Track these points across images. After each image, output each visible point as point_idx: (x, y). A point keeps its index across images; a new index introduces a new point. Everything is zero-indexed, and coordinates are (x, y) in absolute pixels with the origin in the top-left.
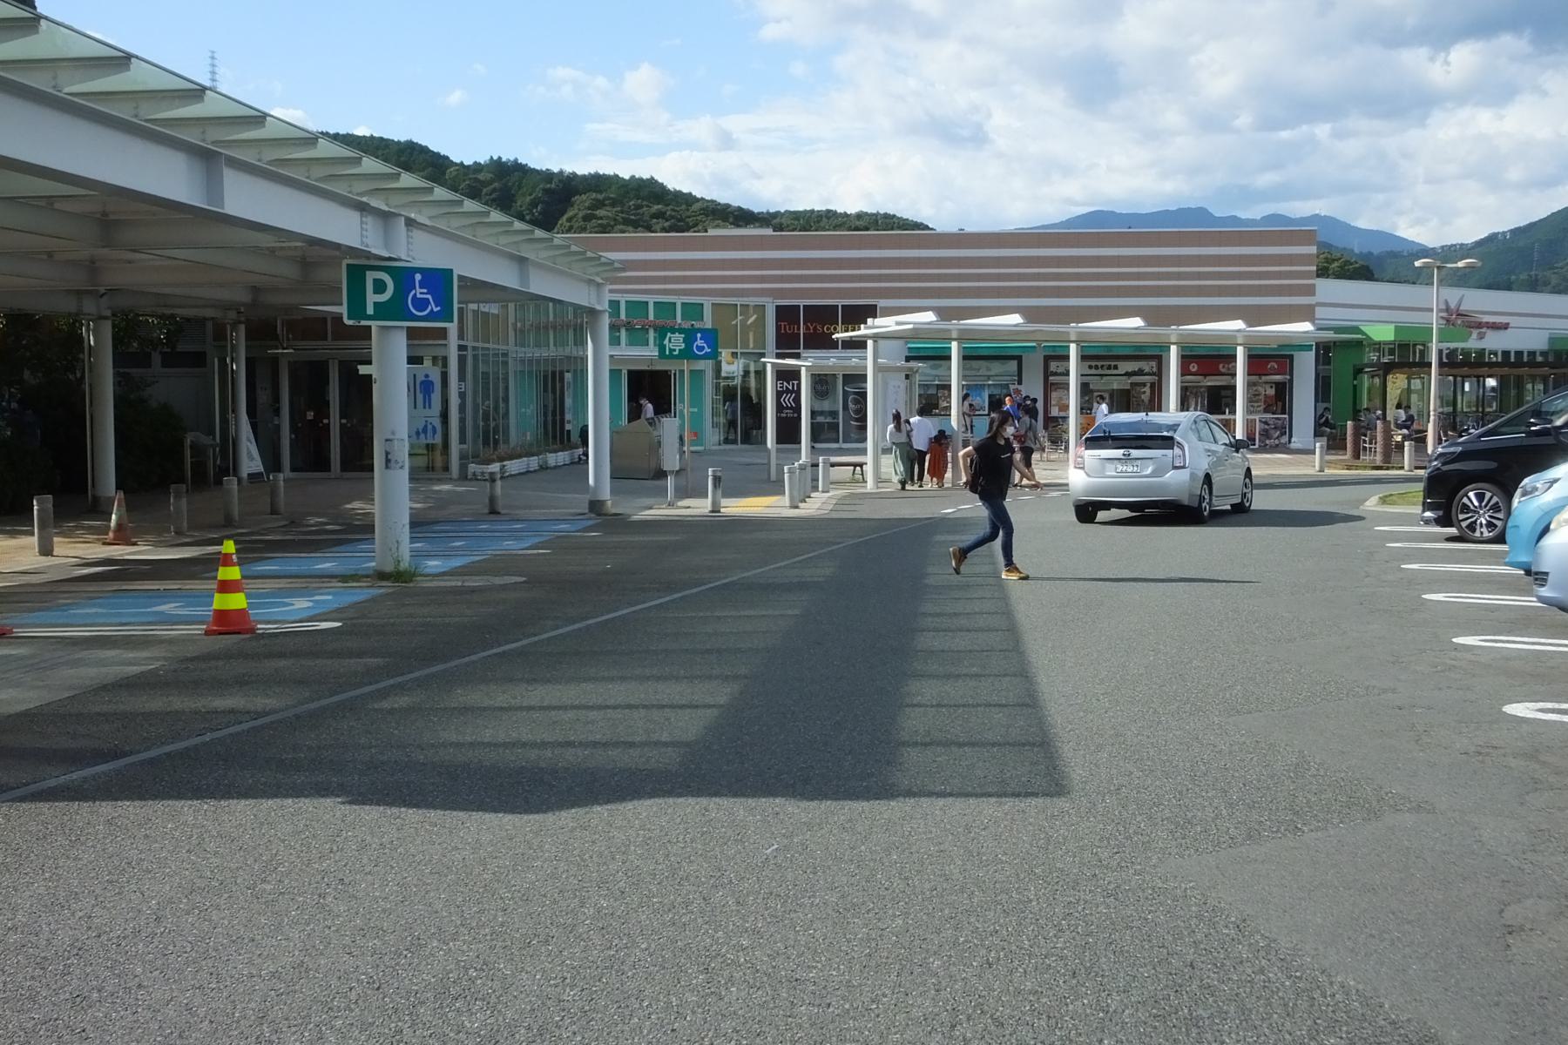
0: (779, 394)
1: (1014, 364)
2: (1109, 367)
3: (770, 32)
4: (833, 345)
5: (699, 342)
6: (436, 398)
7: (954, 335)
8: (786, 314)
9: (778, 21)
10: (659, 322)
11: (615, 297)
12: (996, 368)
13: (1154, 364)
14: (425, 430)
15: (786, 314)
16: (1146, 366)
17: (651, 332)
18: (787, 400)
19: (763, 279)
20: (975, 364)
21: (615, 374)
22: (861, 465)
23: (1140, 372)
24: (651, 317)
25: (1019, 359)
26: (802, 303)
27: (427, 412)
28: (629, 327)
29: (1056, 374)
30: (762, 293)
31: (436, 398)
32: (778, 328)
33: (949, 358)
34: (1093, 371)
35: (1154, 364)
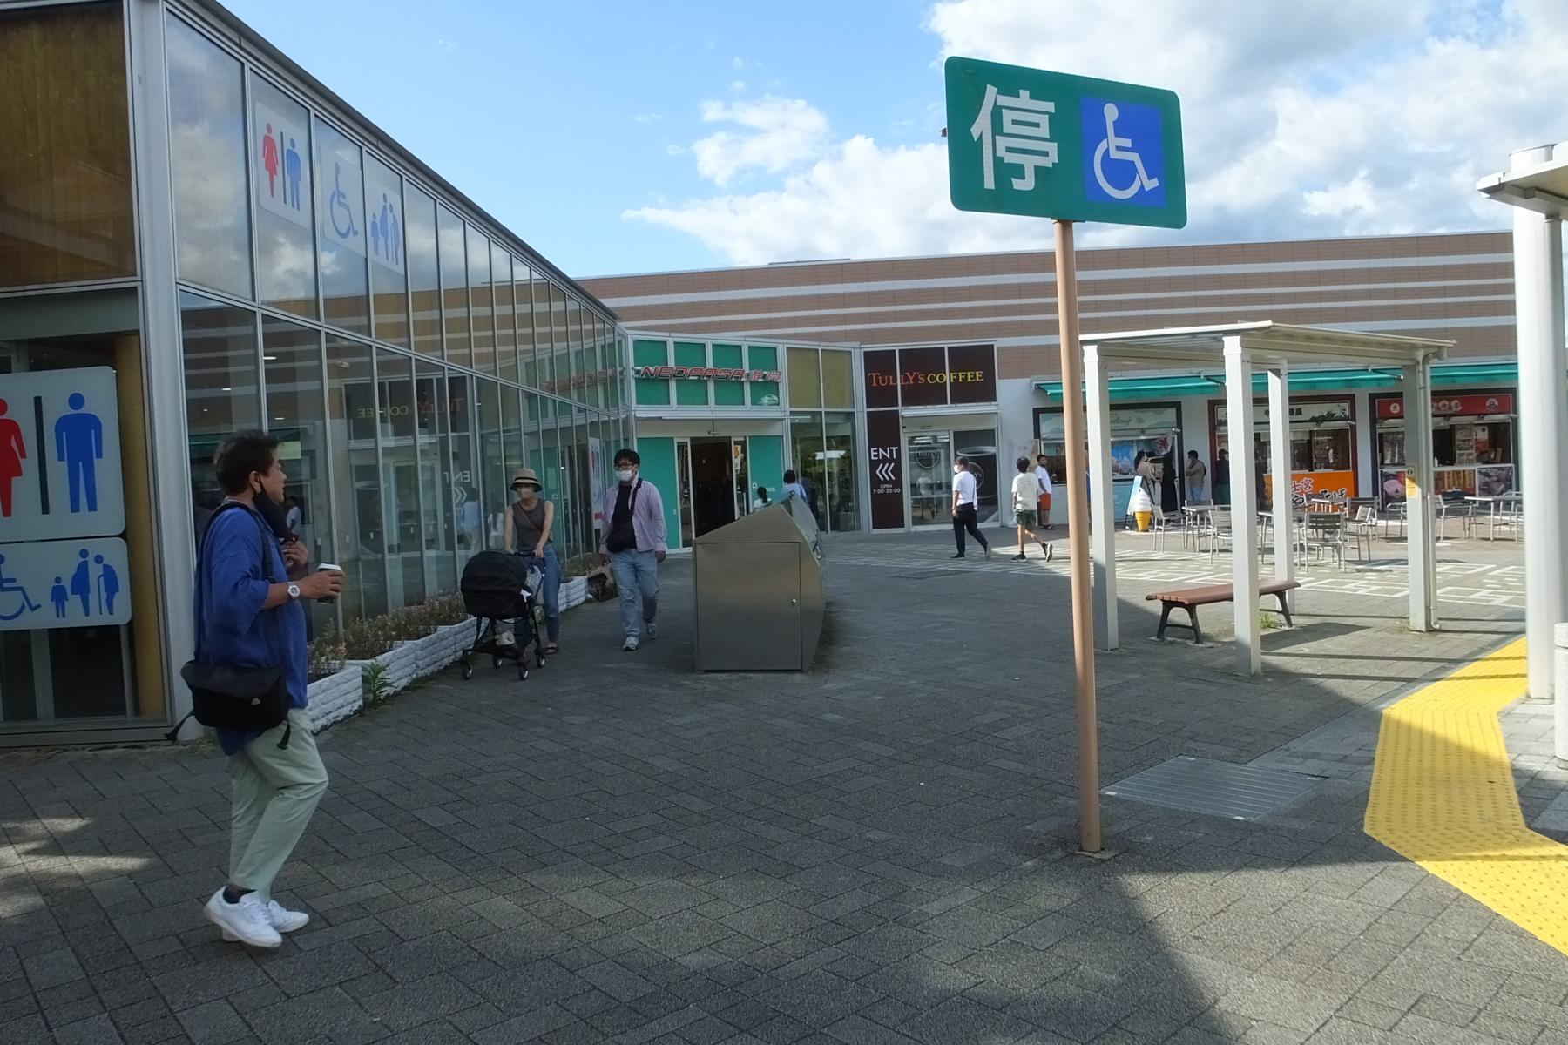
0: (874, 465)
1: (1171, 414)
5: (1114, 145)
6: (107, 470)
8: (877, 363)
10: (722, 372)
12: (1150, 419)
13: (1346, 405)
14: (81, 582)
15: (877, 363)
16: (1336, 409)
17: (711, 386)
18: (885, 472)
19: (845, 319)
20: (1124, 414)
23: (1330, 417)
24: (710, 365)
25: (1177, 406)
26: (897, 347)
27: (86, 522)
30: (846, 336)
31: (107, 470)
32: (868, 380)
33: (1060, 410)
35: (1346, 405)
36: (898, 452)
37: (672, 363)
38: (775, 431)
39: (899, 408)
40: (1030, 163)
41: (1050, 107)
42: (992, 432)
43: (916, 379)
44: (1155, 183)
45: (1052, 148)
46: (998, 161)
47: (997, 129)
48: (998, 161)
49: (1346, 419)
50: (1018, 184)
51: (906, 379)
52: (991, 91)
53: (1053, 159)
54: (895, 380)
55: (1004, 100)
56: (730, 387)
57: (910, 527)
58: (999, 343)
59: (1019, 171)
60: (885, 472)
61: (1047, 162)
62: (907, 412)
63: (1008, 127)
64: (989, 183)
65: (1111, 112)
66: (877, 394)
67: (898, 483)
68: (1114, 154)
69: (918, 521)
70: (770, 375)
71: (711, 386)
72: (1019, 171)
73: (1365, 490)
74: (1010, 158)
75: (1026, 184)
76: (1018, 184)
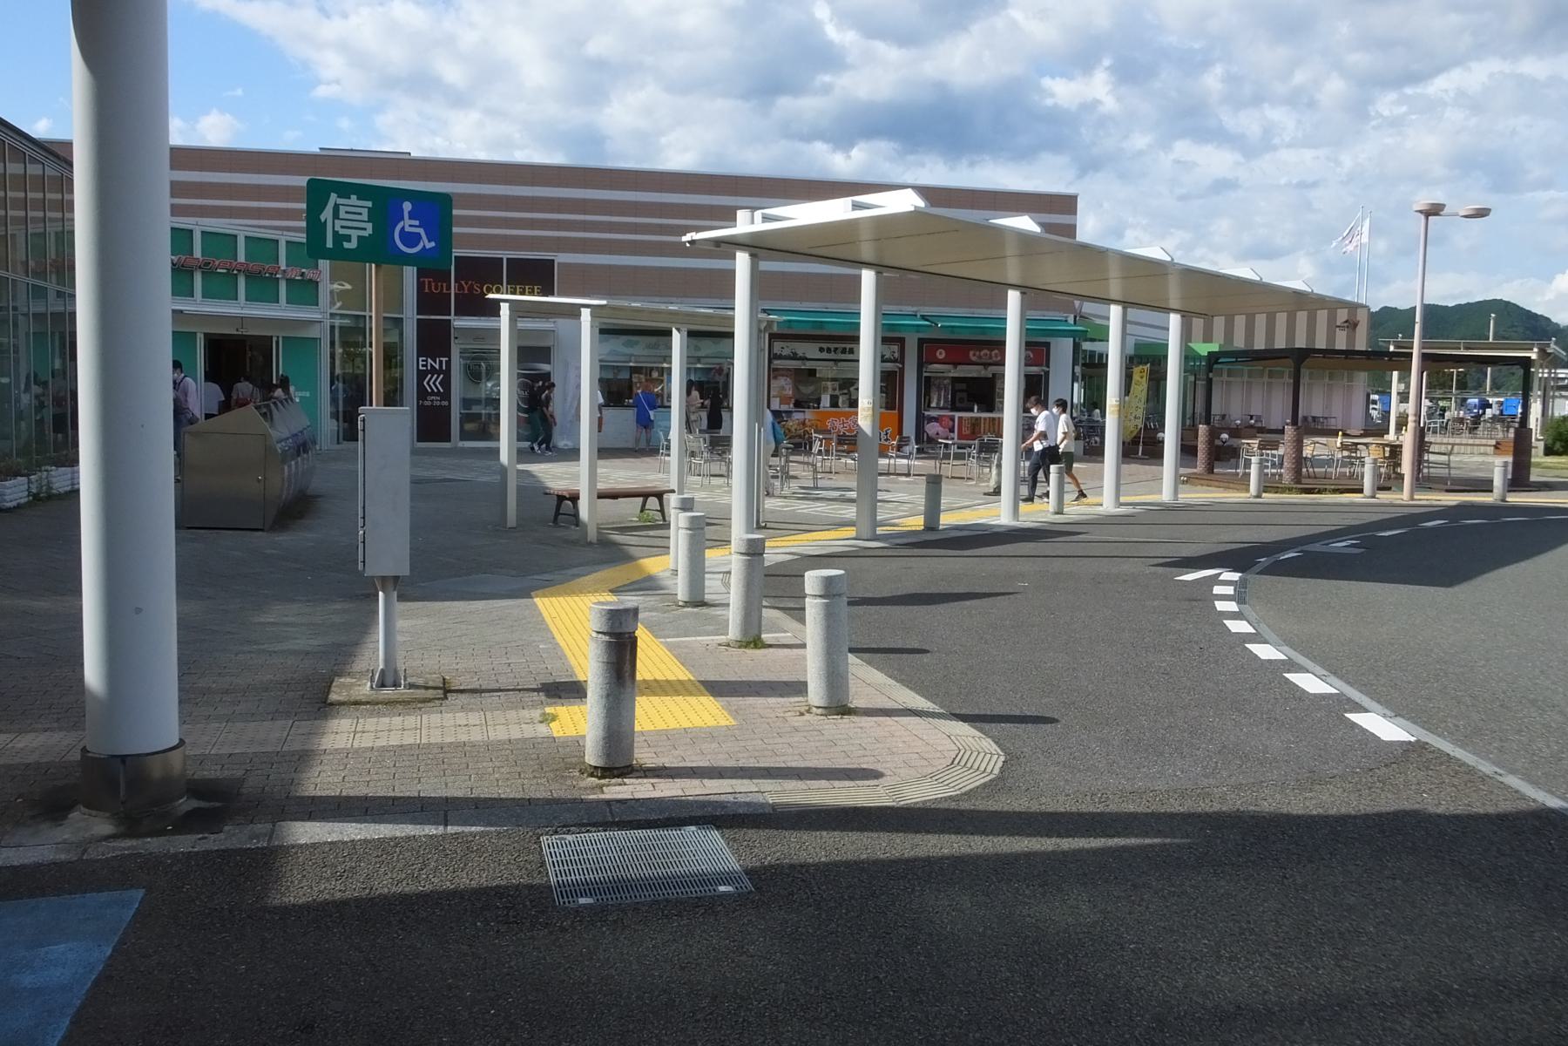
0: (421, 375)
2: (844, 351)
3: (322, 91)
4: (923, 191)
5: (408, 224)
7: (867, 252)
9: (329, 83)
11: (185, 222)
13: (896, 348)
17: (242, 281)
18: (433, 383)
21: (182, 339)
22: (659, 495)
24: (241, 258)
28: (207, 270)
29: (780, 357)
34: (825, 355)
35: (896, 348)
36: (448, 363)
37: (198, 253)
38: (313, 333)
39: (452, 317)
40: (354, 234)
41: (369, 204)
42: (548, 350)
43: (471, 288)
44: (433, 244)
45: (369, 226)
46: (335, 233)
47: (336, 216)
48: (335, 233)
49: (895, 361)
50: (346, 245)
51: (461, 287)
52: (333, 196)
53: (369, 231)
54: (449, 288)
55: (340, 201)
56: (262, 284)
57: (456, 442)
58: (561, 258)
59: (348, 238)
60: (433, 383)
61: (365, 234)
62: (460, 322)
63: (342, 215)
64: (329, 244)
65: (407, 206)
66: (430, 301)
67: (446, 395)
68: (408, 229)
69: (465, 436)
70: (309, 274)
71: (242, 281)
72: (348, 238)
73: (909, 429)
74: (342, 232)
75: (353, 245)
76: (346, 245)
